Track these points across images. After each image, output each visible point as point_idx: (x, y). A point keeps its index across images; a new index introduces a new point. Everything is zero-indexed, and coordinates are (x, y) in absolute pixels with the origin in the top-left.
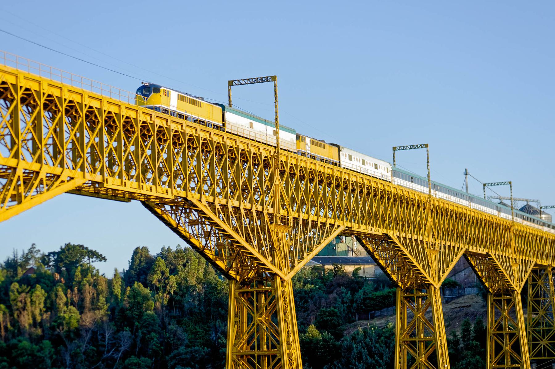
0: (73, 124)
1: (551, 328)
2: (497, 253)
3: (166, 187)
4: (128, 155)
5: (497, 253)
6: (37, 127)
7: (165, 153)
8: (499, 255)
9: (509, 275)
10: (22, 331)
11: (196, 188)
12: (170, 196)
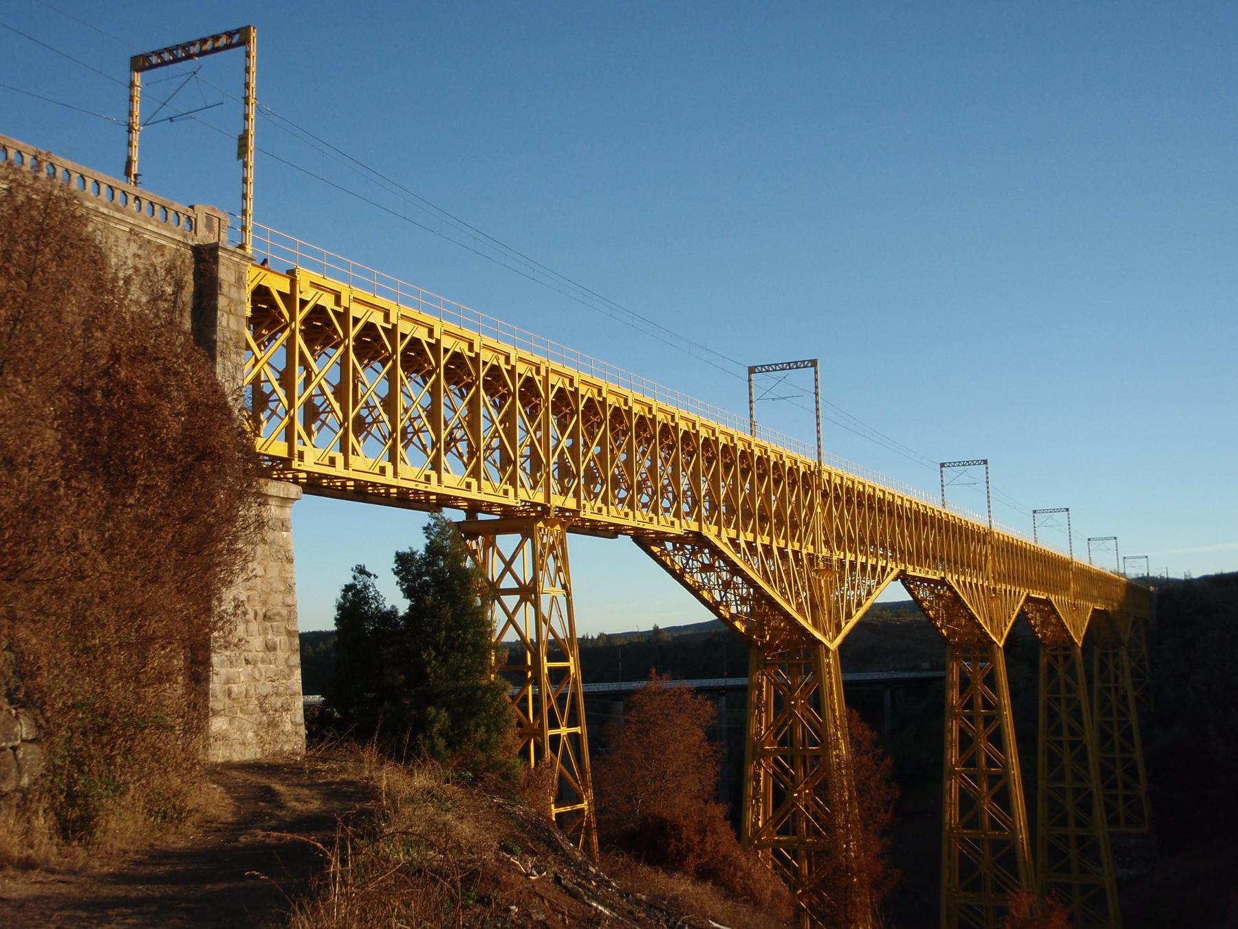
0: (532, 418)
2: (962, 579)
3: (670, 517)
4: (590, 460)
5: (962, 579)
6: (841, 517)
7: (623, 452)
9: (982, 616)
10: (270, 759)
12: (677, 530)
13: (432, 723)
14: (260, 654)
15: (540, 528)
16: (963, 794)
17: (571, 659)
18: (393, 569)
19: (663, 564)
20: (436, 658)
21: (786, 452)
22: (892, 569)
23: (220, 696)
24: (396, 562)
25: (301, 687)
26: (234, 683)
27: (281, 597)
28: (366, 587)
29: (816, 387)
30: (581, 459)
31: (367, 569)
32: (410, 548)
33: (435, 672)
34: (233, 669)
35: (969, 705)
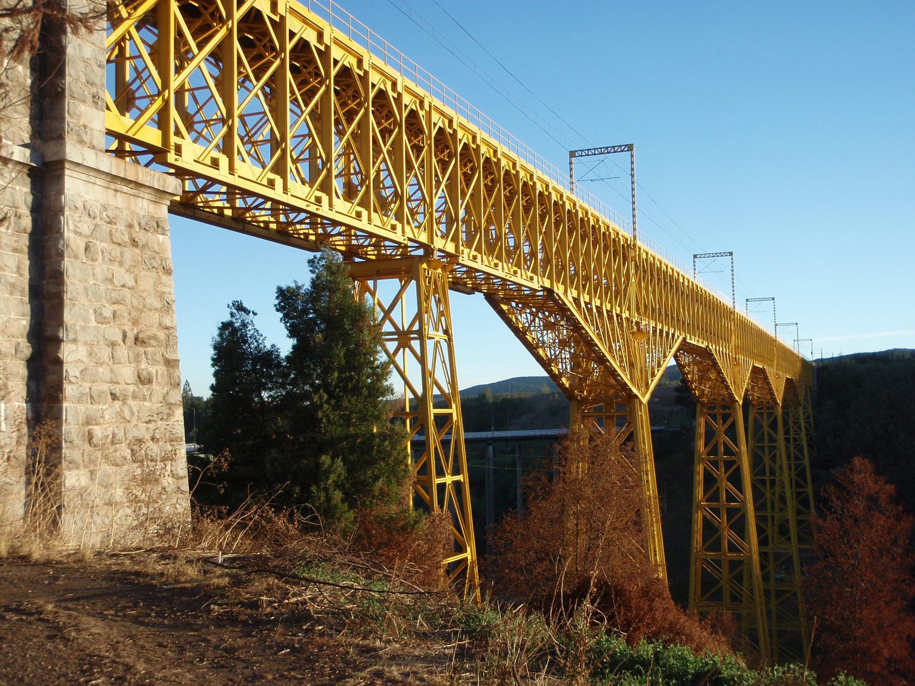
1: (709, 594)
8: (610, 318)
11: (359, 188)
13: (328, 471)
14: (131, 388)
15: (425, 269)
16: (707, 524)
17: (454, 405)
18: (275, 305)
19: (509, 322)
20: (327, 402)
21: (612, 225)
22: (678, 336)
23: (77, 440)
24: (277, 298)
25: (183, 430)
26: (97, 424)
27: (156, 316)
28: (244, 325)
29: (632, 169)
30: (460, 202)
31: (244, 305)
32: (295, 282)
33: (327, 417)
34: (95, 406)
35: (714, 451)
